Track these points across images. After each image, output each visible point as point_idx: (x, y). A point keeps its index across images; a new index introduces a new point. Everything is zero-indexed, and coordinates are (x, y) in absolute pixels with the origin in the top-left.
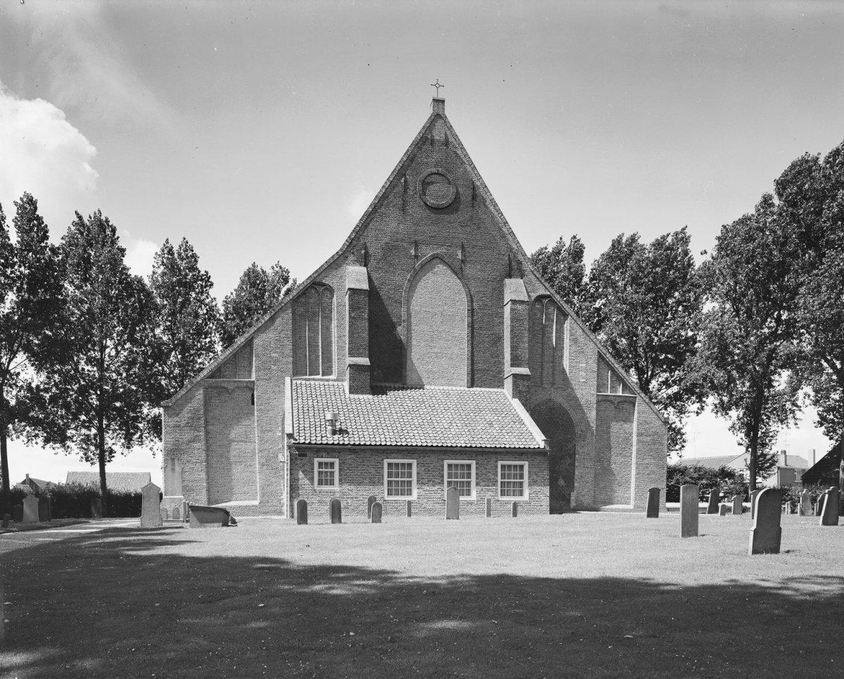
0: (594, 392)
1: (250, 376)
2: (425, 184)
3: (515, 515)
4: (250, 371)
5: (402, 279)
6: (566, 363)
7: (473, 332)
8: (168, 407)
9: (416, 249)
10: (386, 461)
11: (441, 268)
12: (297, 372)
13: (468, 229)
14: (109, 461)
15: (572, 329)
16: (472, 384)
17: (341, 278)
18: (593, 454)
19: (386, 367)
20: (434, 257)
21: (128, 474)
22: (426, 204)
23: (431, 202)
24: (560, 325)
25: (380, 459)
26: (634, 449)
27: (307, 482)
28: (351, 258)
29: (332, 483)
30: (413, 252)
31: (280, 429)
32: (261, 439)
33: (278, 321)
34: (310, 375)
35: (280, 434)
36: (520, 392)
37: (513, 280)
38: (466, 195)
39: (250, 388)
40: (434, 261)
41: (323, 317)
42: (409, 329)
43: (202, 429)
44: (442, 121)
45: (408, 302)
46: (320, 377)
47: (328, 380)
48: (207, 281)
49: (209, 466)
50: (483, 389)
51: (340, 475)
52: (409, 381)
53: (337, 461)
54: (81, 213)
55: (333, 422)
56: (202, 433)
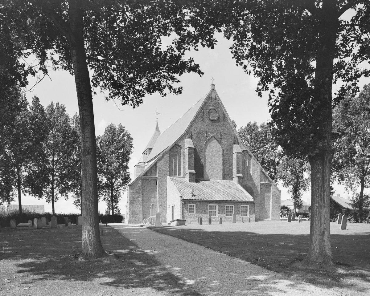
2: (209, 112)
3: (249, 222)
4: (156, 174)
5: (203, 144)
6: (251, 172)
7: (224, 162)
9: (207, 134)
10: (209, 205)
11: (214, 141)
12: (170, 175)
13: (222, 128)
14: (56, 201)
15: (253, 161)
16: (224, 179)
18: (259, 202)
19: (199, 174)
20: (212, 137)
21: (35, 206)
25: (207, 204)
26: (271, 200)
29: (193, 212)
30: (206, 135)
32: (160, 197)
33: (165, 157)
37: (236, 145)
38: (222, 118)
39: (156, 180)
41: (178, 156)
42: (205, 160)
45: (205, 151)
46: (177, 176)
47: (180, 177)
49: (143, 206)
50: (227, 181)
51: (196, 209)
52: (205, 177)
53: (195, 205)
55: (192, 192)
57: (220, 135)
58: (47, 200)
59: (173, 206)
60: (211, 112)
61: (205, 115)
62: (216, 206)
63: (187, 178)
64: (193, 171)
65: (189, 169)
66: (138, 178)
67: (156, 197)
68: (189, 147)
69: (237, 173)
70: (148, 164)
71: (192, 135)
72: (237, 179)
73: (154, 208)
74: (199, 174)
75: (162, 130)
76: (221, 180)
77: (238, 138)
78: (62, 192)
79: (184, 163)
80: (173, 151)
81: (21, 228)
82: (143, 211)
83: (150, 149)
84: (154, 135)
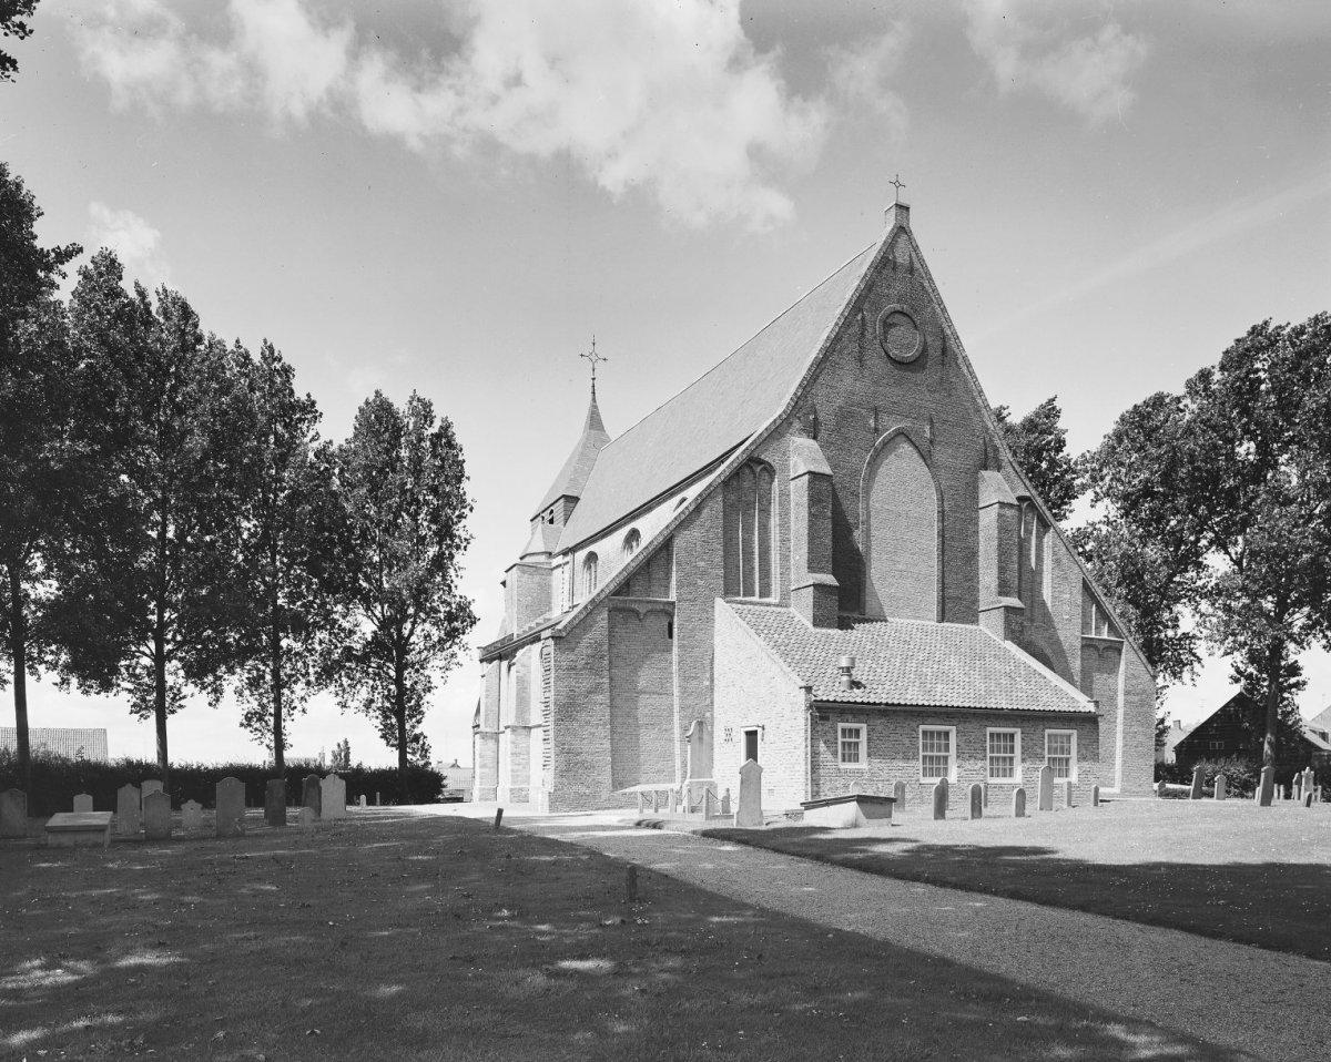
0: (1078, 634)
1: (667, 595)
3: (1308, 805)
4: (667, 587)
6: (1047, 593)
8: (561, 637)
9: (876, 420)
10: (922, 727)
11: (905, 448)
12: (729, 591)
13: (937, 395)
16: (942, 618)
17: (784, 454)
19: (846, 600)
20: (900, 433)
21: (67, 731)
22: (889, 356)
23: (894, 353)
24: (1040, 538)
25: (914, 725)
26: (1120, 712)
27: (830, 757)
28: (797, 425)
30: (872, 422)
31: (708, 676)
32: (684, 690)
33: (706, 512)
34: (745, 595)
35: (708, 683)
36: (1013, 632)
38: (934, 352)
39: (668, 611)
40: (898, 439)
43: (606, 673)
44: (904, 237)
47: (768, 605)
48: (301, 412)
49: (613, 732)
52: (869, 612)
53: (864, 728)
54: (143, 285)
56: (606, 680)
57: (927, 428)
58: (134, 705)
59: (752, 736)
60: (895, 325)
61: (869, 336)
62: (947, 734)
63: (802, 611)
64: (830, 579)
65: (812, 568)
66: (593, 601)
67: (665, 692)
68: (809, 473)
69: (1000, 594)
70: (568, 559)
71: (816, 419)
72: (998, 618)
73: (705, 737)
74: (846, 600)
75: (613, 428)
76: (932, 624)
77: (997, 442)
78: (196, 672)
79: (784, 541)
80: (740, 488)
81: (66, 840)
82: (614, 751)
83: (571, 500)
84: (585, 446)
